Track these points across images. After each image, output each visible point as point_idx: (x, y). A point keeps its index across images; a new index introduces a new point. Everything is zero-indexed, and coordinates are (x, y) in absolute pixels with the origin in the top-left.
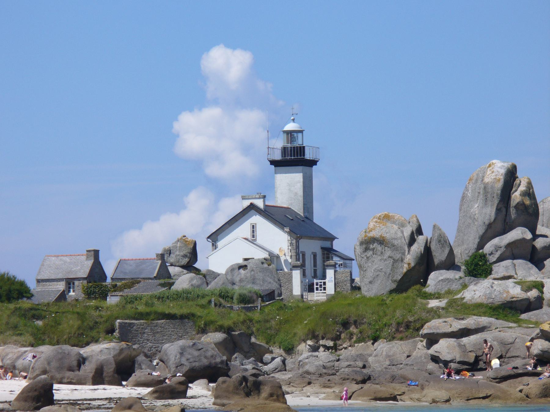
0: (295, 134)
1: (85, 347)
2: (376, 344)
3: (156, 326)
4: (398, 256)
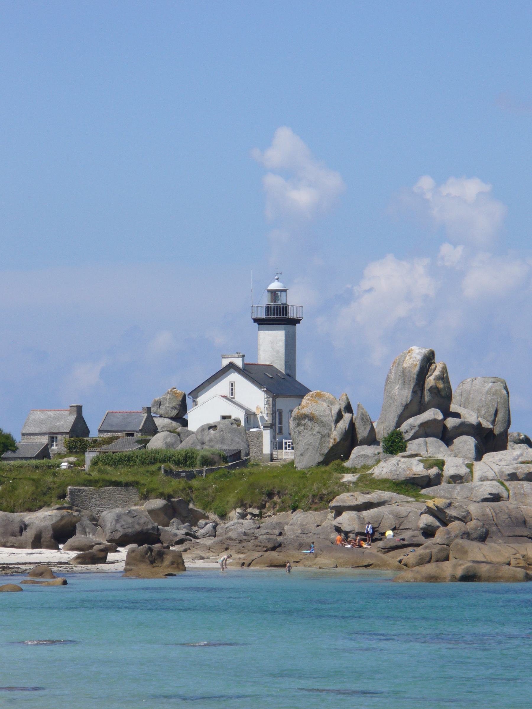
0: (279, 293)
1: (37, 511)
3: (104, 492)
4: (325, 432)
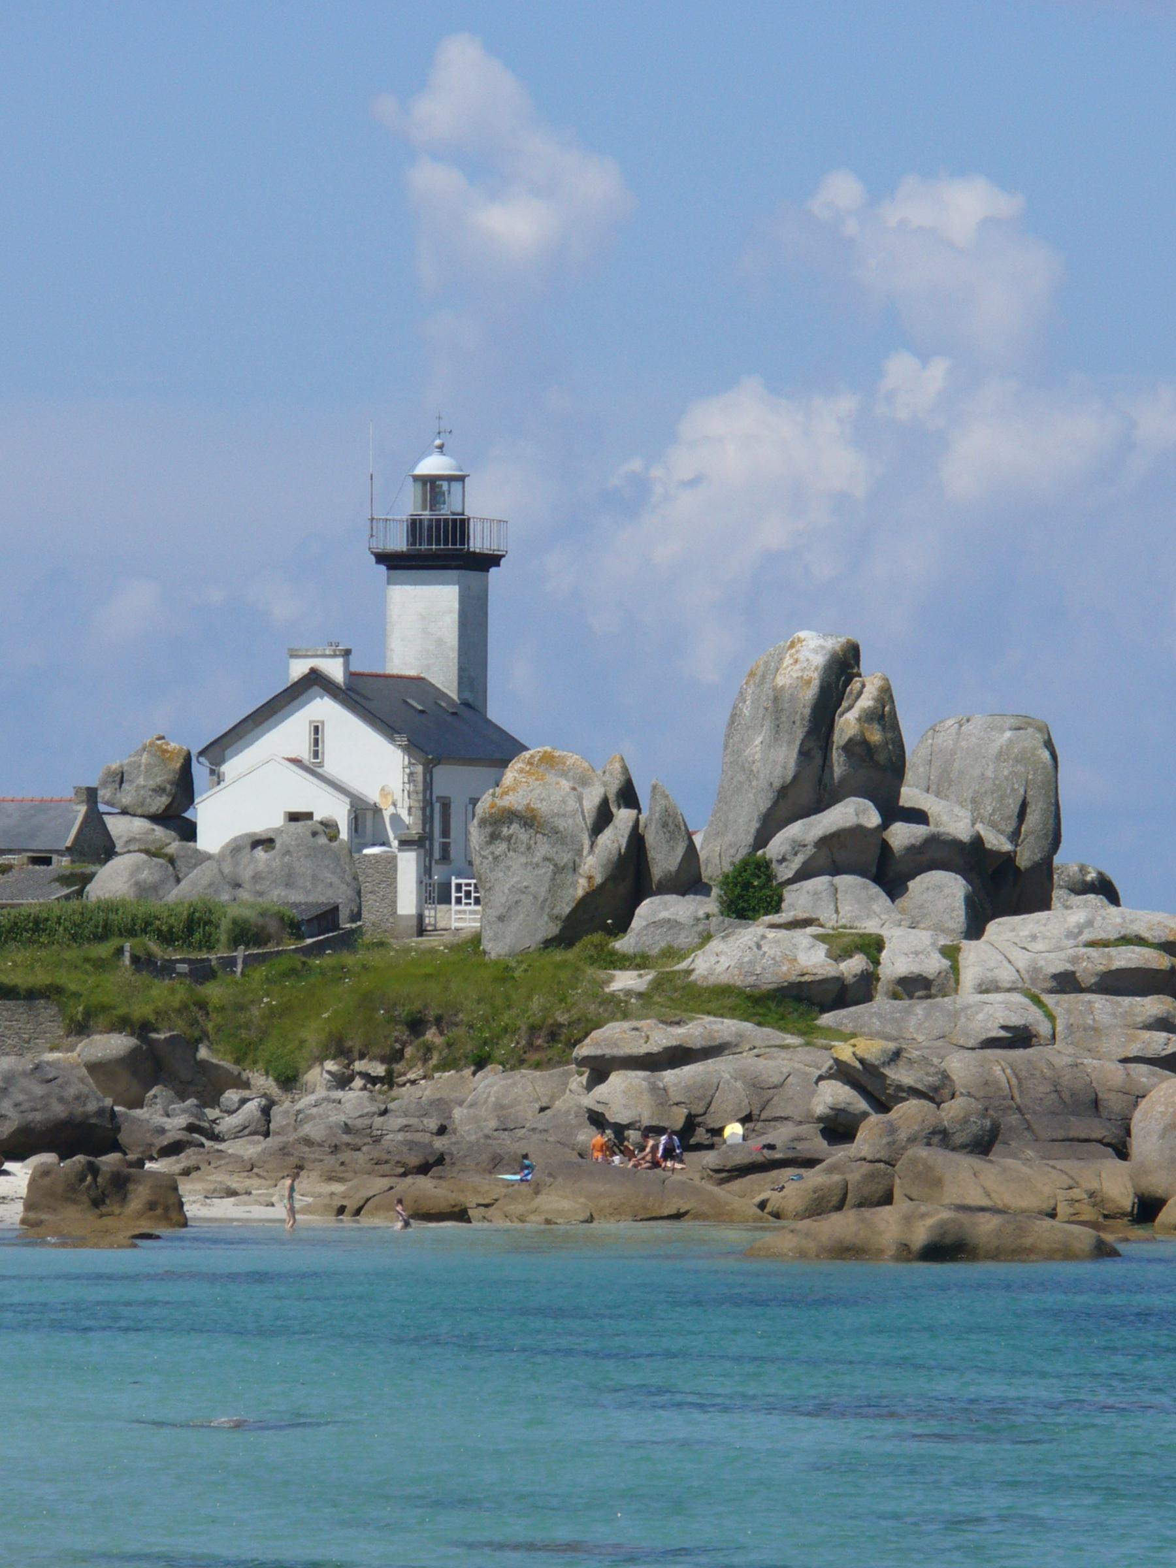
0: (445, 485)
2: (480, 1074)
4: (565, 858)
